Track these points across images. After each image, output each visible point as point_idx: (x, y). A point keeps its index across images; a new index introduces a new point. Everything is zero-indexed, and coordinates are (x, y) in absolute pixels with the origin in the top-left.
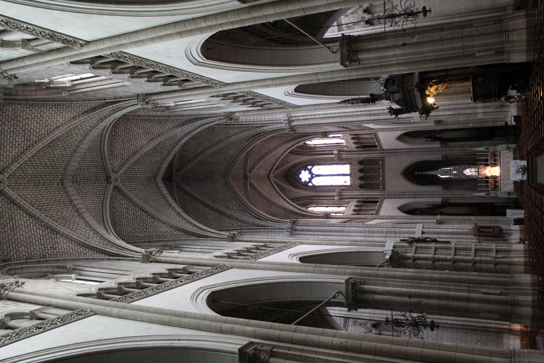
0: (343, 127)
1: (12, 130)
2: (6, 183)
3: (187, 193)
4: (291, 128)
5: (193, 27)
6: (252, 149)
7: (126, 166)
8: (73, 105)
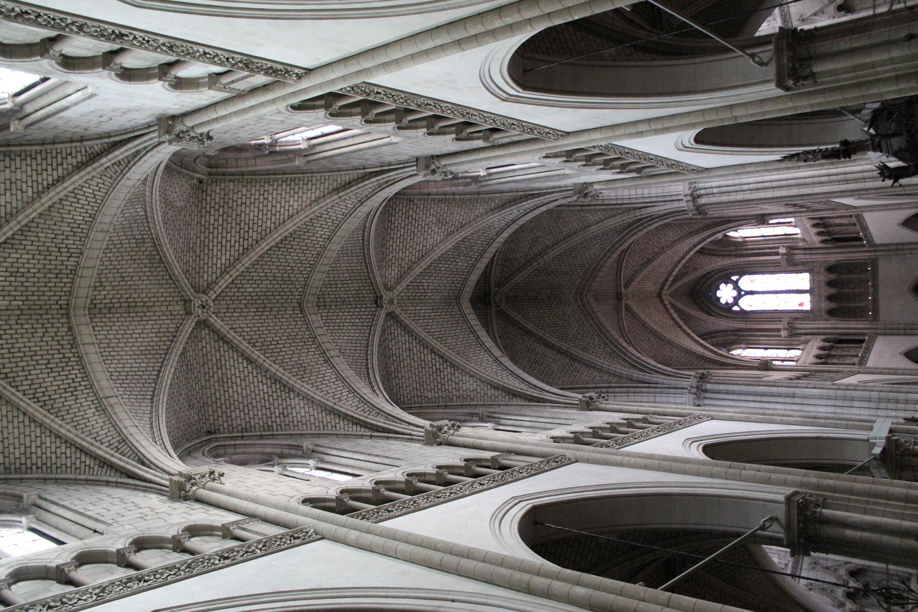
0: (795, 205)
1: (220, 222)
2: (212, 309)
3: (515, 324)
4: (697, 210)
5: (479, 29)
6: (629, 247)
7: (408, 279)
8: (314, 179)
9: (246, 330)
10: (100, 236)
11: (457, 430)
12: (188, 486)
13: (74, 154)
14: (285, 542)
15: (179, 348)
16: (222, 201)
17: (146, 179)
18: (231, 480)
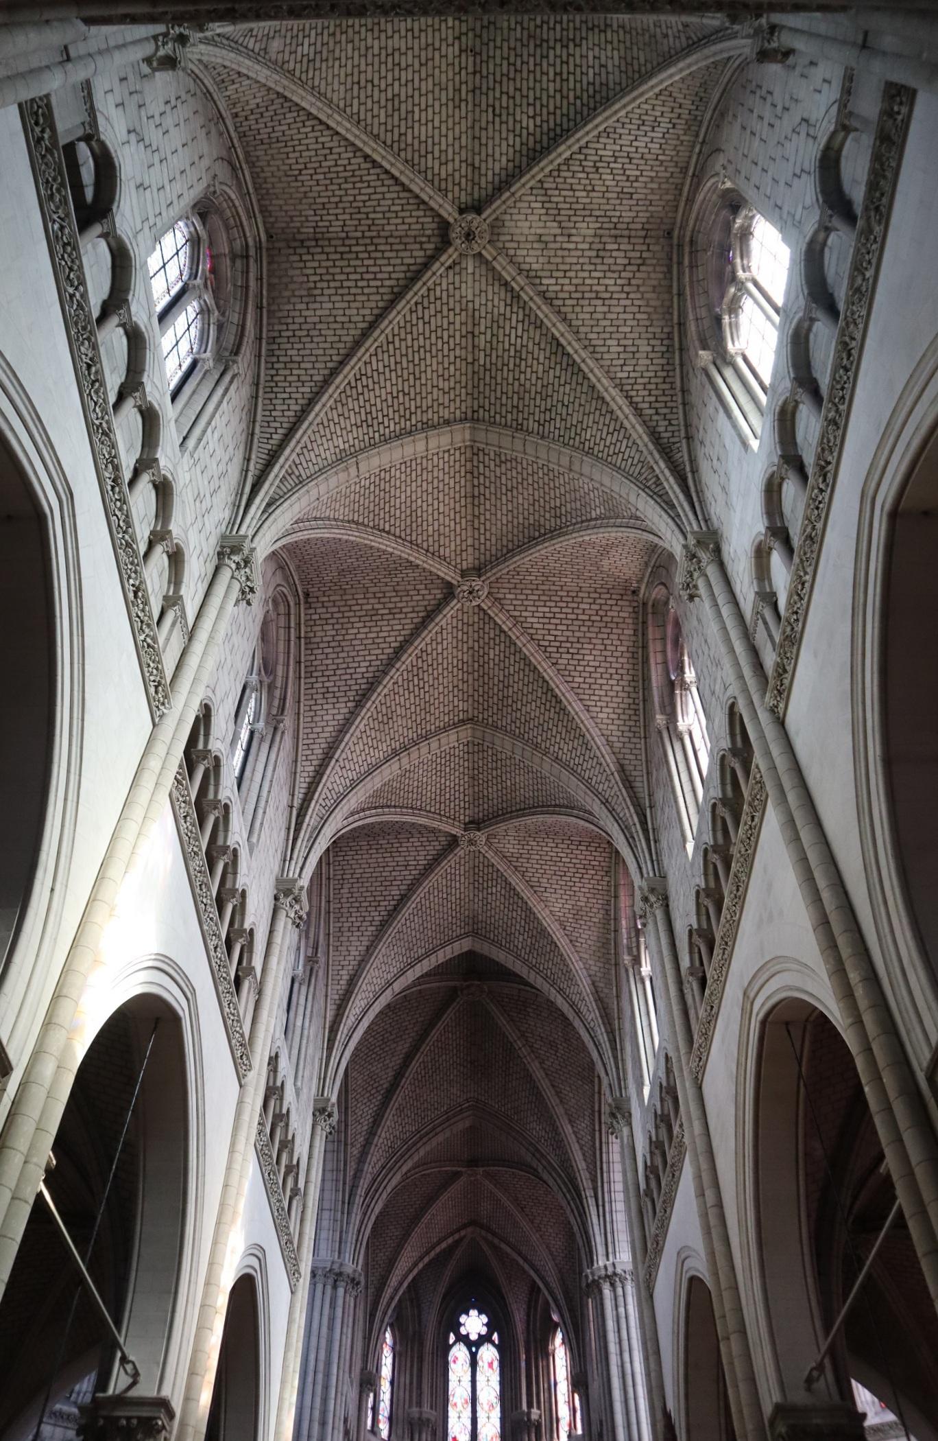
1: (580, 617)
5: (845, 951)
6: (541, 1179)
9: (440, 647)
10: (565, 461)
11: (294, 923)
12: (236, 558)
13: (670, 428)
14: (151, 674)
15: (418, 559)
16: (609, 619)
17: (637, 518)
18: (241, 616)
